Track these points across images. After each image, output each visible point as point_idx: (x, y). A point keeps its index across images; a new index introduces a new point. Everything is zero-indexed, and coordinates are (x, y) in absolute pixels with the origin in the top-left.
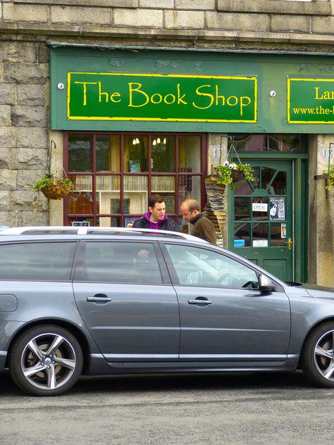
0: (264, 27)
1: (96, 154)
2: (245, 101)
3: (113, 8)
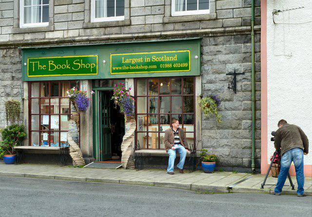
0: (102, 33)
1: (189, 94)
2: (93, 66)
3: (46, 32)
